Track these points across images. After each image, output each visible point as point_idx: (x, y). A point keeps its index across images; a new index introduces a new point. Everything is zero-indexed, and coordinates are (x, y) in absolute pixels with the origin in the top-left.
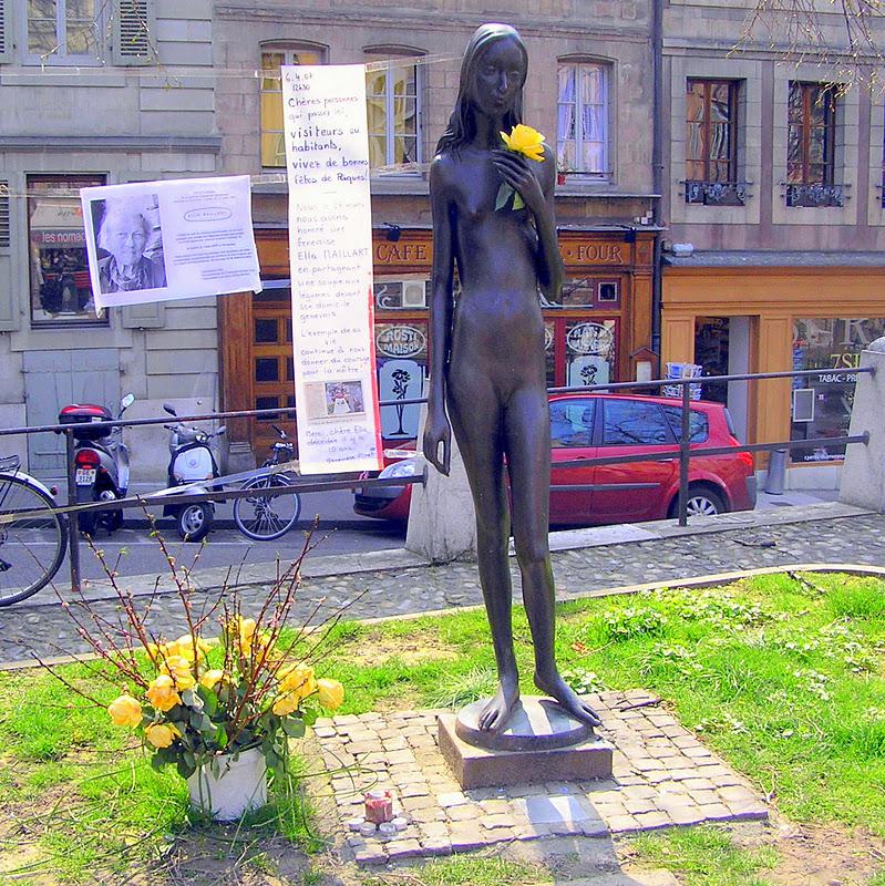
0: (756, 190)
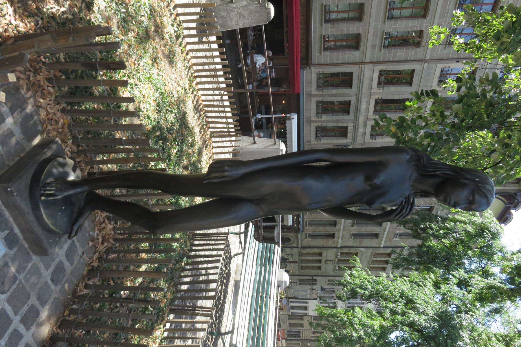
0: (321, 93)
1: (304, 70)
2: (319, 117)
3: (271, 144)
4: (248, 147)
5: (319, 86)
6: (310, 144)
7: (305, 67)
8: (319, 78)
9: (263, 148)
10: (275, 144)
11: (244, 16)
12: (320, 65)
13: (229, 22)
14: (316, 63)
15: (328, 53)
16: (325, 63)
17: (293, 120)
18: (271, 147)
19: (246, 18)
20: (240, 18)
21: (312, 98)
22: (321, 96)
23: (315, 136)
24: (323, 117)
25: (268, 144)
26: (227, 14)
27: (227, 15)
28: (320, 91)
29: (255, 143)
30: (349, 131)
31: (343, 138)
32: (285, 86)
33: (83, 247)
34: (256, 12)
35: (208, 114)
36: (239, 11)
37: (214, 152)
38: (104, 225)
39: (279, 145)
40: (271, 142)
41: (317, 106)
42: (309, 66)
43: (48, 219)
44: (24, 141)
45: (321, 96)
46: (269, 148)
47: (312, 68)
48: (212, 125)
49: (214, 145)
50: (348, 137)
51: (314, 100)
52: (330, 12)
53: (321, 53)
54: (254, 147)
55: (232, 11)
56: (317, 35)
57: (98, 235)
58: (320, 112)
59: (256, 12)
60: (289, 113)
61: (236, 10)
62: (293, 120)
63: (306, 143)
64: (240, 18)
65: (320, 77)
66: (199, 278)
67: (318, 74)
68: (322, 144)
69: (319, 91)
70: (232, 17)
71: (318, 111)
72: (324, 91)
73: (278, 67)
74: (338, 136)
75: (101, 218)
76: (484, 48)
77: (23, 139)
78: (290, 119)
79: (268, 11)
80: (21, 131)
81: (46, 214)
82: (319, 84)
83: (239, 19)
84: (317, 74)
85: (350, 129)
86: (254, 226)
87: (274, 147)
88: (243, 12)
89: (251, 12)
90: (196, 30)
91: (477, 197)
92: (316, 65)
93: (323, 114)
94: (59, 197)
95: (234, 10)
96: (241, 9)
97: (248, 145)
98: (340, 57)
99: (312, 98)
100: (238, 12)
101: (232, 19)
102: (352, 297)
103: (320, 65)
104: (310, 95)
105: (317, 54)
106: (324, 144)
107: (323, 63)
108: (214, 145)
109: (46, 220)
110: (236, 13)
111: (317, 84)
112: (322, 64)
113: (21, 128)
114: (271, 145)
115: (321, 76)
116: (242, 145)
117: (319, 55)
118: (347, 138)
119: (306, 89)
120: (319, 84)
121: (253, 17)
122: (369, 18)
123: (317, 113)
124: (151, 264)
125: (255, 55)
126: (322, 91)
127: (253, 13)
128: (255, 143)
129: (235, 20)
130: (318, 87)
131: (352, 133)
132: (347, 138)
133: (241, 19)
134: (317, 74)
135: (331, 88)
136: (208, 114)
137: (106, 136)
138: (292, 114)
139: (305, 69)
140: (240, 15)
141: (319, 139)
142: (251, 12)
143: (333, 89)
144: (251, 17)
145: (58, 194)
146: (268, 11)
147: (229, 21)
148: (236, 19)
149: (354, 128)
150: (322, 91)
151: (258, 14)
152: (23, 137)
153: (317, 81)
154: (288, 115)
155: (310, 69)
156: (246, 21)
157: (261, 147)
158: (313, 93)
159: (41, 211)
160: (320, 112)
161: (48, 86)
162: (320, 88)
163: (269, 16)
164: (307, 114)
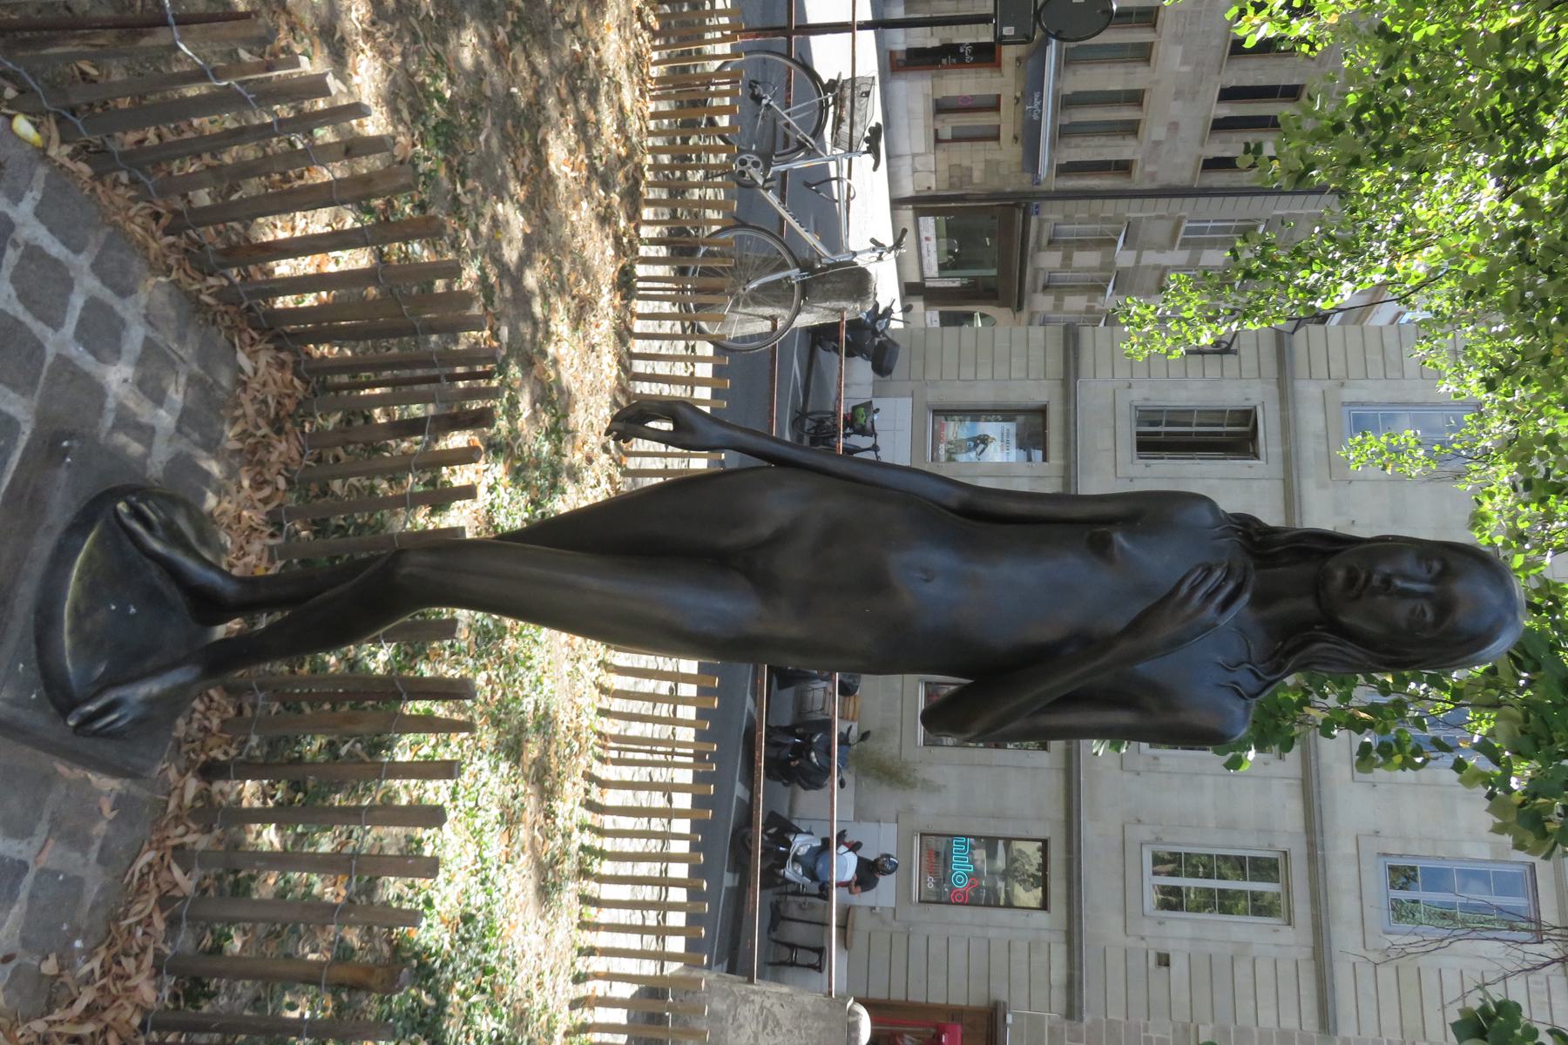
11: (778, 1024)
13: (731, 1035)
19: (784, 1030)
20: (765, 1027)
26: (729, 1007)
27: (729, 1011)
33: (25, 942)
34: (817, 1015)
36: (767, 1004)
43: (79, 579)
55: (745, 1000)
57: (88, 980)
59: (817, 1015)
61: (758, 999)
64: (765, 1027)
66: (456, 342)
70: (742, 1020)
76: (1491, 733)
79: (851, 1019)
81: (90, 557)
83: (760, 1028)
88: (777, 1009)
89: (802, 1014)
90: (625, 1011)
95: (752, 997)
96: (773, 1000)
100: (762, 1008)
101: (740, 1026)
109: (75, 572)
110: (757, 1007)
113: (172, 460)
121: (806, 1028)
124: (341, 347)
127: (806, 1018)
129: (748, 1030)
133: (769, 1029)
140: (767, 1017)
142: (802, 1014)
144: (798, 1027)
145: (160, 533)
146: (851, 1019)
147: (730, 1032)
148: (754, 1027)
151: (822, 1024)
156: (780, 1038)
159: (86, 537)
161: (279, 473)
163: (853, 1035)
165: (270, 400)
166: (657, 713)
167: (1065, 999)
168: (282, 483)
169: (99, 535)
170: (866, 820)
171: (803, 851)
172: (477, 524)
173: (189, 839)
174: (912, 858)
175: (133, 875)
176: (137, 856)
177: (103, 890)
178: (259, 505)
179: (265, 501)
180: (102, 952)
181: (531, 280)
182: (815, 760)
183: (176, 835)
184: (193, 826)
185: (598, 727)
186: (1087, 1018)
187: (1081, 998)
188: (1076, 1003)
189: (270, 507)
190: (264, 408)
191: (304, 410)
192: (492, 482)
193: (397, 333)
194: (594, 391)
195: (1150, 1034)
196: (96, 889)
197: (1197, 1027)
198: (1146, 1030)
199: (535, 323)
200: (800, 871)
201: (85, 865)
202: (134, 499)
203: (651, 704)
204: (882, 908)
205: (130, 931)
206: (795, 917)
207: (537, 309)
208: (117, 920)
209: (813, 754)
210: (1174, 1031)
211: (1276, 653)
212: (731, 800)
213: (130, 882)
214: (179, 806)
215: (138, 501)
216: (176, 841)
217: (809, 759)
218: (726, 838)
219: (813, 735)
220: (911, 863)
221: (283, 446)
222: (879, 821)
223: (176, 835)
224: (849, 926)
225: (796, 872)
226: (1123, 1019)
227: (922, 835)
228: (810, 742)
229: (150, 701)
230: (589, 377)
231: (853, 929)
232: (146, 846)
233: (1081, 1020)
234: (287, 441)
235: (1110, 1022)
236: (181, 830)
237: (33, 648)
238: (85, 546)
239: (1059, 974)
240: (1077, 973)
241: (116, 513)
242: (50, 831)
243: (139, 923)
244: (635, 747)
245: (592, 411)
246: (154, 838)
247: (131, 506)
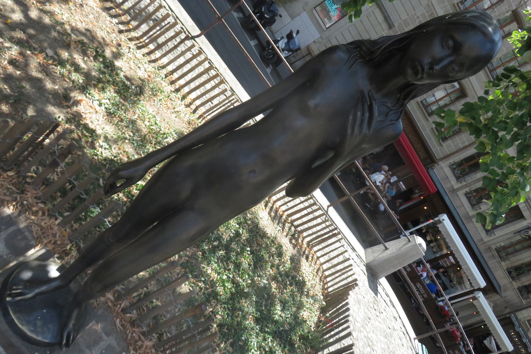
0: (464, 183)
1: (433, 169)
2: (477, 209)
3: (404, 243)
4: (381, 256)
5: (459, 177)
6: (484, 243)
7: (432, 166)
8: (453, 170)
9: (398, 251)
10: (409, 241)
12: (447, 157)
14: (442, 156)
15: (449, 142)
16: (452, 152)
17: (444, 221)
18: (407, 246)
21: (458, 193)
22: (466, 186)
23: (484, 232)
24: (481, 207)
25: (401, 244)
28: (462, 181)
29: (386, 249)
30: (522, 209)
31: (519, 220)
32: (417, 191)
35: (296, 223)
37: (322, 262)
38: (140, 343)
39: (415, 240)
40: (404, 241)
41: (469, 199)
42: (436, 163)
43: (23, 325)
44: (10, 255)
45: (466, 186)
46: (404, 247)
47: (441, 163)
48: (305, 234)
49: (319, 254)
50: (526, 217)
51: (461, 194)
52: (429, 105)
53: (441, 145)
54: (388, 252)
56: (428, 131)
58: (475, 203)
60: (437, 216)
62: (444, 221)
63: (478, 244)
65: (455, 168)
67: (451, 166)
68: (498, 237)
69: (461, 183)
71: (473, 203)
72: (466, 179)
73: (405, 178)
74: (513, 221)
75: (134, 335)
77: (9, 254)
78: (440, 222)
80: (6, 246)
82: (457, 175)
84: (449, 166)
85: (524, 207)
86: (424, 347)
87: (410, 245)
91: (459, 37)
92: (442, 158)
93: (480, 205)
94: (30, 296)
97: (380, 254)
98: (465, 139)
99: (458, 193)
102: (265, 237)
103: (447, 157)
104: (454, 191)
105: (438, 148)
106: (501, 236)
107: (449, 153)
108: (319, 254)
109: (20, 326)
111: (455, 176)
112: (449, 155)
114: (406, 244)
115: (454, 167)
116: (374, 256)
117: (441, 147)
118: (525, 219)
119: (446, 186)
120: (457, 175)
122: (473, 90)
123: (473, 206)
125: (372, 175)
126: (465, 181)
128: (386, 249)
130: (458, 178)
131: (528, 211)
132: (525, 219)
134: (449, 166)
135: (473, 173)
136: (296, 223)
137: (298, 326)
138: (439, 216)
139: (433, 167)
141: (491, 233)
143: (476, 174)
145: (27, 291)
149: (527, 204)
150: (465, 181)
152: (8, 251)
153: (454, 173)
154: (436, 219)
155: (438, 165)
157: (394, 250)
158: (455, 187)
159: (10, 315)
160: (475, 203)
162: (461, 179)
164: (461, 212)
165: (9, 186)
166: (211, 75)
167: (386, 24)
168: (42, 205)
169: (13, 310)
170: (295, 17)
171: (284, 46)
172: (107, 120)
173: (123, 306)
174: (315, 17)
175: (119, 327)
176: (115, 324)
177: (116, 340)
178: (43, 218)
179: (44, 214)
180: (131, 348)
181: (34, 14)
182: (267, 17)
183: (118, 308)
184: (120, 302)
185: (197, 116)
186: (396, 25)
187: (392, 21)
188: (390, 23)
189: (46, 214)
190: (11, 190)
191: (21, 176)
192: (98, 102)
193: (15, 143)
194: (97, 19)
195: (417, 15)
196: (114, 341)
197: (431, 2)
198: (416, 15)
199: (53, 27)
200: (287, 52)
201: (106, 341)
202: (8, 292)
203: (207, 74)
204: (317, 39)
205: (132, 337)
206: (294, 61)
207: (47, 20)
208: (126, 339)
209: (266, 15)
210: (425, 8)
211: (399, 99)
212: (252, 48)
213: (120, 329)
214: (112, 302)
215: (10, 291)
216: (120, 309)
217: (266, 18)
218: (259, 59)
219: (261, 9)
220: (317, 19)
221: (29, 194)
222: (299, 15)
223: (118, 308)
224: (311, 51)
225: (286, 53)
226: (407, 17)
227: (315, 8)
228: (262, 12)
229: (74, 325)
230: (91, 16)
231: (313, 52)
232: (115, 318)
233: (394, 26)
234: (28, 192)
235: (403, 21)
236: (118, 306)
237: (33, 346)
238: (13, 317)
239: (380, 18)
240: (386, 14)
241: (9, 302)
242: (90, 350)
243: (132, 334)
244: (211, 111)
245: (104, 26)
246: (114, 315)
247: (10, 295)
